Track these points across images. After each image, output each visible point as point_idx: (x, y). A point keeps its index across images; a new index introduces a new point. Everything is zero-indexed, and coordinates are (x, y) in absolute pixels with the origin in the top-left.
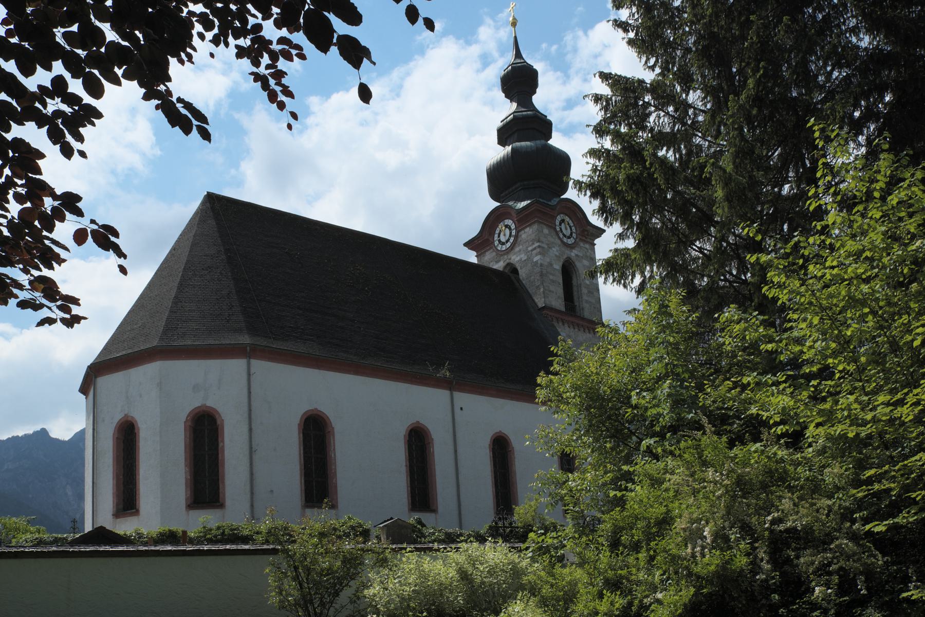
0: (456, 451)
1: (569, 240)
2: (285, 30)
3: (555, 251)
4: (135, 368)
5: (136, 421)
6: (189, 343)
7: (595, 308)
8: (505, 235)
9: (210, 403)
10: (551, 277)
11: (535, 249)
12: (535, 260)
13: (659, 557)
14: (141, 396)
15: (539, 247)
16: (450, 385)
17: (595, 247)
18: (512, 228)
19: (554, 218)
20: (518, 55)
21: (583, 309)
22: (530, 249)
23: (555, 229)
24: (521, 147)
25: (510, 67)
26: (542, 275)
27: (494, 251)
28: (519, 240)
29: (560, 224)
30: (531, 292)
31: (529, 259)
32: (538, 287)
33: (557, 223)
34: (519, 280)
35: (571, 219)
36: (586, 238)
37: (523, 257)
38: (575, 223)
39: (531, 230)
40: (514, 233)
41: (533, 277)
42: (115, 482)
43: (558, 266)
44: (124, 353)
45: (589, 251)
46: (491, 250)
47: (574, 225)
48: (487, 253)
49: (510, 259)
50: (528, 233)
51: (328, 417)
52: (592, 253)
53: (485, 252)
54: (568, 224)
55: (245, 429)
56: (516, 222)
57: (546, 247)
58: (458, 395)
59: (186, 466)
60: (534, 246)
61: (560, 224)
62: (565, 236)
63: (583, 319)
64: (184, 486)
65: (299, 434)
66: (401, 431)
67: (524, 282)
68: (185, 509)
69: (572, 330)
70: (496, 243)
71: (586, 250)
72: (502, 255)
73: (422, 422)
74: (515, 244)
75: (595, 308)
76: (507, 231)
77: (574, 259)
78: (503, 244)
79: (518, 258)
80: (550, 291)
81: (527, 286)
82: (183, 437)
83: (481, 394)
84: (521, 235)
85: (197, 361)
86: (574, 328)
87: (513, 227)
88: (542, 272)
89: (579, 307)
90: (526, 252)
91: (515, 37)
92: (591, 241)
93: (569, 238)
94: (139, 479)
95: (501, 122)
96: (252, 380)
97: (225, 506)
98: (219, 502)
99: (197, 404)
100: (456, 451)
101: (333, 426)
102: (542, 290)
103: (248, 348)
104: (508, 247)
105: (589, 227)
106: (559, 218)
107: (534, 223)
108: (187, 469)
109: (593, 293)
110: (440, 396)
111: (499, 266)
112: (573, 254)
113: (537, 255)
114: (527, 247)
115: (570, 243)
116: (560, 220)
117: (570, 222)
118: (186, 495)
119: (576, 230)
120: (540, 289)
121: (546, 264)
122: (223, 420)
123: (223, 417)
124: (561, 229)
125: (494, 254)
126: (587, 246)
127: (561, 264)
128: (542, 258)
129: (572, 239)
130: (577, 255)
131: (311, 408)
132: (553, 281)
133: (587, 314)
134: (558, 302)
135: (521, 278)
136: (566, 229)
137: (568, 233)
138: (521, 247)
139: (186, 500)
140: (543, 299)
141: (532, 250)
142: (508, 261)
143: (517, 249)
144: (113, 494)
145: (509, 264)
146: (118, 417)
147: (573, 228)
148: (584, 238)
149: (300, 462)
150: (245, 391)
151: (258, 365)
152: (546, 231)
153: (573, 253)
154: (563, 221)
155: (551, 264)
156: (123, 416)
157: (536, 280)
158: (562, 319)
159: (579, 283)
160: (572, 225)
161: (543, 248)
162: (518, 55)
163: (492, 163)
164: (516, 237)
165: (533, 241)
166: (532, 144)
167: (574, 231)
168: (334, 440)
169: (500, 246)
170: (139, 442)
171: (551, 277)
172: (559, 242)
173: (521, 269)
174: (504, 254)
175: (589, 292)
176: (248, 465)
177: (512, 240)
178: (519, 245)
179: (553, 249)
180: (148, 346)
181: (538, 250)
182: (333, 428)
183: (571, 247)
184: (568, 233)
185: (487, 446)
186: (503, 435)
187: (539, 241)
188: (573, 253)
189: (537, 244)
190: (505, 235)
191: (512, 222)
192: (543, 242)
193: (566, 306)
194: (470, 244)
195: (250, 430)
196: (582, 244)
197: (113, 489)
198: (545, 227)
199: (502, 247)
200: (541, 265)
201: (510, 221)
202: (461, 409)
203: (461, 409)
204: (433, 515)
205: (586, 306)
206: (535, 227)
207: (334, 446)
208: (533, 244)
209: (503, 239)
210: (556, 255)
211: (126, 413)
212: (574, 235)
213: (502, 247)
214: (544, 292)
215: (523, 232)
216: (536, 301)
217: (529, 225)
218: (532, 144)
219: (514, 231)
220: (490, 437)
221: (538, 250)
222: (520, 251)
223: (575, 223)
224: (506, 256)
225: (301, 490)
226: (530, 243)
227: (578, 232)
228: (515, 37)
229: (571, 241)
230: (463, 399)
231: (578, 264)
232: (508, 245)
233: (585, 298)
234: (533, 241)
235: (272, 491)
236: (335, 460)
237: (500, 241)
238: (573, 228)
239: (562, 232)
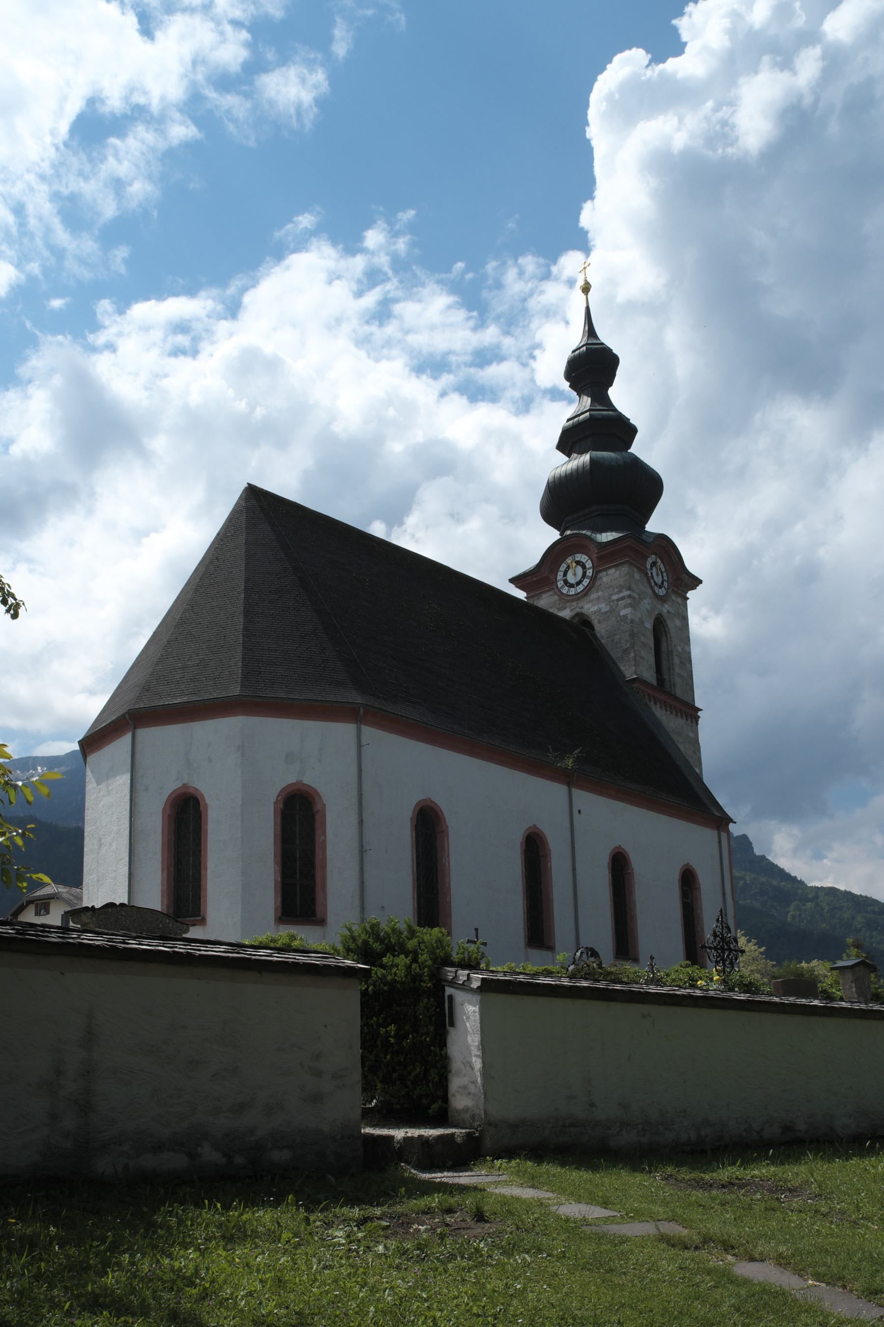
0: (574, 869)
1: (660, 590)
2: (436, 275)
3: (646, 603)
4: (201, 722)
5: (202, 795)
6: (282, 695)
7: (687, 684)
8: (575, 575)
9: (307, 780)
10: (643, 639)
11: (623, 598)
12: (623, 613)
13: (167, 921)
14: (210, 761)
15: (630, 596)
16: (568, 779)
17: (688, 602)
18: (588, 566)
19: (646, 558)
20: (591, 331)
21: (674, 685)
22: (614, 597)
23: (646, 574)
24: (603, 458)
25: (585, 348)
26: (632, 635)
27: (555, 593)
28: (598, 583)
29: (651, 569)
30: (613, 656)
31: (611, 611)
32: (626, 651)
33: (649, 567)
34: (595, 636)
35: (662, 562)
36: (678, 589)
37: (604, 607)
38: (668, 568)
39: (618, 572)
40: (589, 573)
41: (617, 637)
42: (165, 876)
43: (649, 625)
44: (185, 699)
45: (682, 607)
46: (552, 593)
47: (666, 571)
48: (544, 596)
49: (582, 608)
50: (612, 576)
51: (441, 811)
52: (684, 609)
53: (542, 593)
54: (660, 569)
55: (354, 819)
56: (595, 560)
57: (637, 597)
58: (576, 792)
59: (275, 863)
60: (621, 595)
61: (651, 569)
62: (656, 584)
63: (675, 698)
64: (273, 890)
65: (412, 831)
66: (518, 838)
67: (603, 641)
68: (273, 922)
69: (664, 711)
70: (560, 584)
71: (677, 605)
72: (568, 601)
73: (540, 826)
74: (590, 589)
75: (687, 684)
76: (579, 570)
77: (665, 616)
78: (571, 586)
79: (595, 608)
80: (642, 658)
81: (608, 648)
82: (271, 823)
83: (599, 792)
84: (601, 578)
85: (290, 720)
86: (666, 710)
87: (589, 564)
88: (633, 630)
89: (670, 681)
90: (609, 601)
91: (588, 309)
92: (683, 593)
93: (660, 587)
94: (206, 875)
95: (568, 420)
96: (363, 752)
97: (326, 924)
98: (316, 917)
99: (292, 780)
100: (574, 869)
101: (448, 824)
102: (632, 655)
103: (362, 710)
104: (579, 591)
105: (684, 575)
106: (650, 561)
107: (623, 563)
108: (277, 868)
109: (685, 665)
110: (556, 791)
111: (566, 614)
112: (665, 611)
113: (625, 607)
114: (611, 595)
115: (661, 594)
116: (651, 562)
117: (662, 566)
118: (275, 903)
119: (668, 578)
120: (629, 653)
121: (637, 620)
122: (325, 805)
123: (325, 799)
124: (652, 573)
125: (556, 598)
126: (679, 600)
127: (652, 621)
128: (633, 612)
129: (663, 589)
130: (668, 612)
131: (424, 798)
132: (644, 644)
133: (678, 692)
134: (650, 676)
135: (599, 635)
136: (658, 575)
137: (659, 580)
138: (600, 593)
139: (276, 909)
140: (634, 668)
141: (618, 600)
142: (578, 610)
143: (594, 596)
144: (162, 892)
145: (577, 614)
146: (171, 786)
147: (665, 574)
148: (676, 589)
149: (413, 871)
150: (354, 769)
151: (369, 732)
152: (637, 576)
153: (665, 608)
154: (654, 564)
155: (642, 622)
156: (180, 785)
157: (623, 641)
158: (654, 697)
159: (670, 649)
160: (663, 570)
161: (634, 598)
162: (591, 331)
163: (557, 475)
164: (593, 579)
165: (621, 589)
166: (618, 456)
167: (666, 578)
168: (448, 843)
169: (566, 588)
170: (206, 824)
171: (643, 639)
172: (650, 591)
173: (599, 622)
174: (573, 601)
175: (681, 662)
176: (357, 869)
177: (586, 582)
178: (597, 591)
179: (644, 600)
180: (223, 694)
181: (629, 601)
182: (447, 827)
183: (663, 599)
184: (659, 580)
185: (606, 864)
186: (622, 851)
187: (630, 589)
188: (665, 608)
189: (628, 593)
190: (575, 575)
191: (587, 558)
192: (633, 591)
193: (657, 680)
194: (516, 581)
195: (361, 822)
196: (673, 597)
197: (162, 885)
198: (635, 570)
199: (569, 591)
200: (632, 621)
201: (584, 556)
202: (579, 811)
203: (579, 811)
204: (550, 953)
205: (678, 680)
206: (625, 569)
207: (448, 850)
208: (620, 591)
209: (571, 579)
210: (647, 609)
211: (185, 781)
212: (665, 583)
213: (569, 591)
214: (635, 659)
215: (604, 573)
216: (623, 668)
217: (616, 566)
218: (618, 456)
219: (591, 571)
220: (609, 852)
221: (629, 601)
222: (599, 598)
223: (668, 568)
224: (575, 604)
225: (414, 909)
226: (616, 590)
227: (670, 581)
228: (588, 309)
229: (662, 592)
230: (584, 799)
231: (670, 624)
232: (580, 588)
233: (677, 670)
234: (621, 589)
235: (383, 907)
236: (449, 870)
237: (566, 582)
238: (665, 574)
239: (653, 578)
